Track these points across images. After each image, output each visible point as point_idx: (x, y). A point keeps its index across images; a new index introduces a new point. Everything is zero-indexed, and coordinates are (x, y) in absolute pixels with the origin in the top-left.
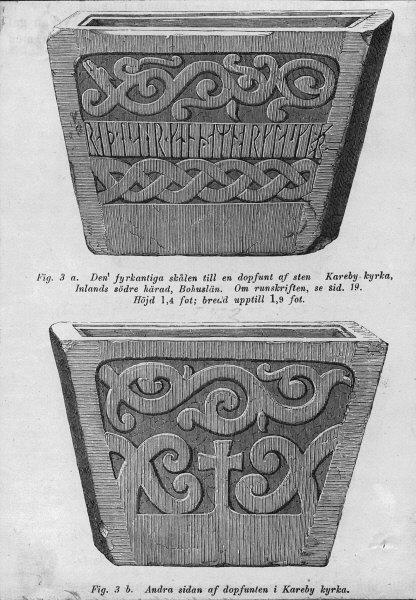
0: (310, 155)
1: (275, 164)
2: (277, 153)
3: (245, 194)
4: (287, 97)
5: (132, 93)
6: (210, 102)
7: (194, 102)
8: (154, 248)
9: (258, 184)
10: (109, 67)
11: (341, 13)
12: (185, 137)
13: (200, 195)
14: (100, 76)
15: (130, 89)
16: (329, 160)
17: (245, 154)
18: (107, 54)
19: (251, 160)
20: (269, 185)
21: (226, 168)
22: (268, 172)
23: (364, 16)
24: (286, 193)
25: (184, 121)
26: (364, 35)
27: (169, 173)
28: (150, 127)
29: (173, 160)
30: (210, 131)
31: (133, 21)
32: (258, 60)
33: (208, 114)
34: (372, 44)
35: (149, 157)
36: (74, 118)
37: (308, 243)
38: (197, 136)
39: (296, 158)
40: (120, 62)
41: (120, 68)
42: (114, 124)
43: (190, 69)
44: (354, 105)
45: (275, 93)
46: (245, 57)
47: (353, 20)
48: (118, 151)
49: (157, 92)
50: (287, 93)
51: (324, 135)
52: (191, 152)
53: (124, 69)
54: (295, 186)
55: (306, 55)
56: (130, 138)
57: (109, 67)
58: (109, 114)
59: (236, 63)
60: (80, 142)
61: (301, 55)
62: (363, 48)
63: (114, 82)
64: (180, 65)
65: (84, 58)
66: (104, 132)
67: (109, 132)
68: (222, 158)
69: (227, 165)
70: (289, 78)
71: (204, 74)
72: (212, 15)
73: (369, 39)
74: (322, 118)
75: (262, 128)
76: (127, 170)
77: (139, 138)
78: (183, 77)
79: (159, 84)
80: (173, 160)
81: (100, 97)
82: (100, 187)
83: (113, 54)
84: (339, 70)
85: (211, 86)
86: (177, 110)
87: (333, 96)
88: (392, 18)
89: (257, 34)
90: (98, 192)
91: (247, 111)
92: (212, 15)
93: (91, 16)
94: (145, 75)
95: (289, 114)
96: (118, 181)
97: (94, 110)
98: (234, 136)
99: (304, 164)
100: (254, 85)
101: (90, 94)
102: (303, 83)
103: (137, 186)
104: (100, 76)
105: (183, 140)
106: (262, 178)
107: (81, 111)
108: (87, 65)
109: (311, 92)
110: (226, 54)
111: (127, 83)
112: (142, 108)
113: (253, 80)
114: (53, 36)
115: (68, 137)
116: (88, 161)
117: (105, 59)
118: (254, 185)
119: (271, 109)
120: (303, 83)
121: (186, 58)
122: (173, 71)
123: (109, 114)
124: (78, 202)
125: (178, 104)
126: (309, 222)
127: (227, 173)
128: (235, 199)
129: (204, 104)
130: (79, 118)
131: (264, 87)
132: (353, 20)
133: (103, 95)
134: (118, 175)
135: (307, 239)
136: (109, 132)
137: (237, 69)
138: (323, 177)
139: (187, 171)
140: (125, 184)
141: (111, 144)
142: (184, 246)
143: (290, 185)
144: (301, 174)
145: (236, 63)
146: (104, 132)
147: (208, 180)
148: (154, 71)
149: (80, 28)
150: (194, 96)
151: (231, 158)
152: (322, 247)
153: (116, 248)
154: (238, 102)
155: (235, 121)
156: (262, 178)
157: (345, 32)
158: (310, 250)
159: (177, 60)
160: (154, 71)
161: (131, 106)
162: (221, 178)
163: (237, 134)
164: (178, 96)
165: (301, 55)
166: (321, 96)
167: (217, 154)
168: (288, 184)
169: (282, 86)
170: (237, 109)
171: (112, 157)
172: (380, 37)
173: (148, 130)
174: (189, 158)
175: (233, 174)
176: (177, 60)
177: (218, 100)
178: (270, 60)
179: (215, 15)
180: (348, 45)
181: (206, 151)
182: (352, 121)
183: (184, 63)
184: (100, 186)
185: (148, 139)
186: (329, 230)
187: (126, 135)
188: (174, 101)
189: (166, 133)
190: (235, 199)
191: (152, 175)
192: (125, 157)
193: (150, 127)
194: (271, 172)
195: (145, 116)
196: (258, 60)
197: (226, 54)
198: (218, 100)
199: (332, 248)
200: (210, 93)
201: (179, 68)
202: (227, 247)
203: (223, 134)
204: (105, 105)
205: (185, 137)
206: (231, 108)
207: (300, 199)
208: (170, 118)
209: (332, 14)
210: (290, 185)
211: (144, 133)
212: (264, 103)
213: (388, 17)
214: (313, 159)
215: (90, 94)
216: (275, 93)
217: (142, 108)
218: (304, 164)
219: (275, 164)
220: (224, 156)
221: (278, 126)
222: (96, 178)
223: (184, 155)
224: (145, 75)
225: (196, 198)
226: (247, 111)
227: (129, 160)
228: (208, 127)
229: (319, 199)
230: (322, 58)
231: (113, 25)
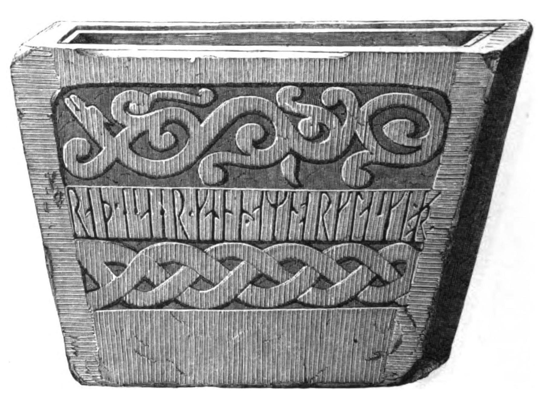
0: (407, 237)
1: (355, 250)
2: (357, 233)
3: (310, 294)
4: (373, 152)
5: (140, 144)
6: (255, 158)
7: (234, 158)
8: (171, 375)
9: (328, 281)
10: (104, 107)
11: (452, 25)
12: (219, 209)
13: (240, 296)
14: (92, 119)
15: (136, 139)
16: (435, 239)
17: (309, 235)
18: (101, 85)
19: (317, 244)
20: (344, 283)
21: (281, 256)
22: (341, 262)
23: (486, 29)
24: (371, 294)
25: (217, 185)
26: (488, 57)
27: (196, 262)
28: (167, 196)
29: (199, 244)
30: (257, 201)
31: (140, 36)
32: (327, 96)
33: (255, 174)
34: (499, 71)
35: (165, 239)
36: (52, 182)
37: (403, 369)
38: (236, 210)
39: (384, 242)
40: (121, 97)
41: (122, 102)
42: (110, 191)
43: (228, 108)
44: (472, 162)
45: (354, 144)
46: (309, 91)
47: (470, 35)
48: (117, 228)
49: (177, 141)
50: (372, 144)
51: (428, 206)
52: (228, 233)
53: (126, 108)
54: (385, 283)
55: (404, 88)
56: (136, 211)
57: (104, 107)
58: (102, 177)
59: (295, 99)
60: (58, 217)
61: (394, 87)
62: (485, 77)
63: (112, 127)
64: (211, 103)
65: (66, 91)
66: (95, 200)
67: (103, 202)
68: (275, 241)
69: (284, 251)
70: (376, 120)
71: (244, 116)
72: (259, 27)
73: (495, 63)
74: (425, 182)
75: (335, 198)
76: (131, 259)
77: (149, 211)
78: (213, 121)
79: (179, 131)
80: (199, 244)
81: (91, 150)
82: (91, 285)
83: (110, 85)
84: (449, 108)
85: (259, 134)
86: (207, 170)
87: (441, 149)
88: (529, 32)
89: (327, 56)
90: (87, 291)
91: (312, 172)
92: (259, 27)
93: (76, 29)
94: (156, 118)
95: (376, 174)
96: (117, 275)
97: (82, 170)
98: (292, 208)
99: (396, 251)
100: (323, 131)
101: (76, 145)
102: (395, 130)
103: (146, 283)
104: (92, 119)
105: (215, 215)
106: (334, 271)
107: (60, 170)
108: (72, 102)
109: (406, 142)
110: (280, 85)
111: (131, 130)
112: (152, 166)
113: (321, 125)
114: (21, 59)
115: (42, 209)
116: (72, 247)
117: (99, 93)
118: (322, 282)
119: (348, 170)
120: (395, 130)
121: (221, 91)
122: (199, 111)
123: (102, 177)
124: (57, 306)
125: (209, 159)
126: (405, 333)
127: (281, 263)
128: (294, 302)
129: (247, 161)
130: (58, 181)
131: (338, 134)
132: (470, 35)
133: (95, 147)
134: (117, 266)
135: (402, 364)
136: (103, 202)
137: (299, 107)
138: (426, 271)
139: (222, 261)
140: (125, 282)
141: (106, 220)
142: (219, 370)
143: (377, 281)
144: (394, 264)
145: (295, 99)
146: (95, 200)
147: (252, 273)
148: (173, 112)
149: (63, 46)
150: (232, 149)
151: (287, 241)
152: (425, 375)
153: (115, 374)
154: (299, 158)
155: (295, 187)
156: (334, 271)
157: (458, 54)
158: (407, 378)
159: (206, 96)
160: (173, 112)
161: (132, 161)
162: (271, 269)
163: (296, 206)
164: (207, 151)
165: (394, 87)
166: (424, 149)
167: (266, 236)
168: (374, 280)
169: (364, 133)
170: (297, 169)
171: (107, 239)
172: (512, 59)
173: (163, 200)
174: (223, 240)
175: (290, 265)
176: (206, 96)
177: (268, 154)
178: (347, 95)
179: (452, 25)
180: (461, 74)
181: (250, 230)
182: (470, 187)
183: (216, 100)
184: (90, 283)
185: (162, 212)
186: (435, 349)
187: (130, 208)
188: (201, 156)
189: (191, 204)
190: (294, 302)
191: (167, 266)
192: (129, 239)
193: (167, 196)
194: (346, 262)
195: (154, 179)
196: (327, 96)
197: (280, 85)
198: (268, 154)
199: (440, 377)
200: (257, 144)
201: (209, 106)
202: (285, 376)
203: (275, 206)
204: (99, 162)
205: (219, 209)
206: (287, 168)
207: (392, 303)
208: (195, 181)
209: (441, 26)
210: (377, 281)
211: (156, 206)
212: (338, 158)
213: (521, 31)
214: (412, 242)
215: (76, 145)
216: (354, 144)
217: (152, 166)
218: (396, 251)
219: (355, 250)
220: (278, 238)
221: (358, 193)
222: (84, 272)
223: (218, 235)
224: (156, 118)
225: (236, 302)
226: (312, 172)
227: (134, 244)
228: (252, 195)
229: (421, 303)
230: (423, 92)
231: (109, 42)
